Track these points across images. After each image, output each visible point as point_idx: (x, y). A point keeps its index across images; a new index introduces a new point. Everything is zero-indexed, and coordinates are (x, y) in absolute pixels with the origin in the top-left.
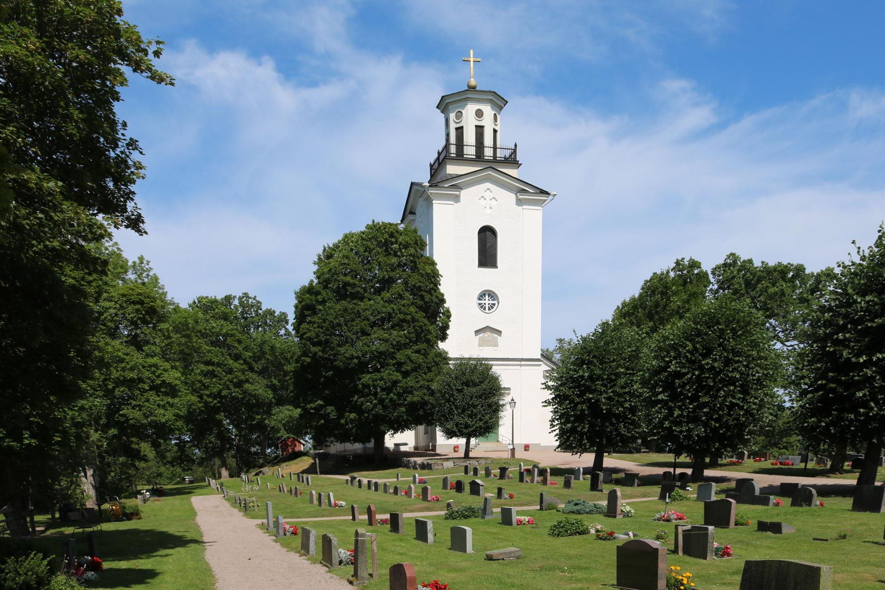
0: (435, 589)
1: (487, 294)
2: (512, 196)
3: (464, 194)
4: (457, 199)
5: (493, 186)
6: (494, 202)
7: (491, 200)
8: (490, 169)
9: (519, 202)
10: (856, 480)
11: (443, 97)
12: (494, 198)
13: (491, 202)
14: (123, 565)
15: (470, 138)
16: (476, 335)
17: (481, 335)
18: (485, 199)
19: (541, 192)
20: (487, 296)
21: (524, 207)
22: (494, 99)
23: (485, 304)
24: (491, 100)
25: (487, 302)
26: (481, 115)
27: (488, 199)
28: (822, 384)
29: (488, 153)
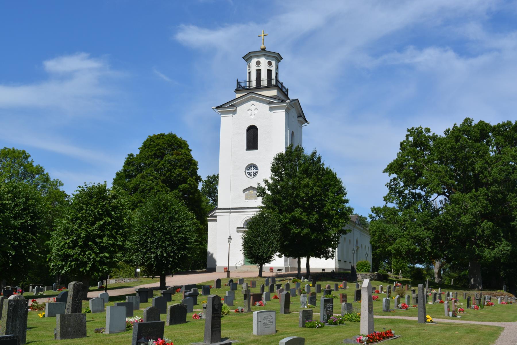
0: (516, 144)
1: (252, 166)
2: (267, 107)
3: (239, 109)
4: (234, 112)
6: (256, 111)
7: (254, 110)
9: (271, 109)
10: (159, 283)
11: (250, 52)
12: (256, 109)
13: (255, 111)
15: (264, 76)
16: (244, 192)
17: (247, 192)
18: (251, 110)
20: (252, 167)
21: (274, 111)
22: (278, 57)
23: (251, 170)
25: (252, 171)
27: (253, 110)
28: (3, 292)
29: (264, 83)
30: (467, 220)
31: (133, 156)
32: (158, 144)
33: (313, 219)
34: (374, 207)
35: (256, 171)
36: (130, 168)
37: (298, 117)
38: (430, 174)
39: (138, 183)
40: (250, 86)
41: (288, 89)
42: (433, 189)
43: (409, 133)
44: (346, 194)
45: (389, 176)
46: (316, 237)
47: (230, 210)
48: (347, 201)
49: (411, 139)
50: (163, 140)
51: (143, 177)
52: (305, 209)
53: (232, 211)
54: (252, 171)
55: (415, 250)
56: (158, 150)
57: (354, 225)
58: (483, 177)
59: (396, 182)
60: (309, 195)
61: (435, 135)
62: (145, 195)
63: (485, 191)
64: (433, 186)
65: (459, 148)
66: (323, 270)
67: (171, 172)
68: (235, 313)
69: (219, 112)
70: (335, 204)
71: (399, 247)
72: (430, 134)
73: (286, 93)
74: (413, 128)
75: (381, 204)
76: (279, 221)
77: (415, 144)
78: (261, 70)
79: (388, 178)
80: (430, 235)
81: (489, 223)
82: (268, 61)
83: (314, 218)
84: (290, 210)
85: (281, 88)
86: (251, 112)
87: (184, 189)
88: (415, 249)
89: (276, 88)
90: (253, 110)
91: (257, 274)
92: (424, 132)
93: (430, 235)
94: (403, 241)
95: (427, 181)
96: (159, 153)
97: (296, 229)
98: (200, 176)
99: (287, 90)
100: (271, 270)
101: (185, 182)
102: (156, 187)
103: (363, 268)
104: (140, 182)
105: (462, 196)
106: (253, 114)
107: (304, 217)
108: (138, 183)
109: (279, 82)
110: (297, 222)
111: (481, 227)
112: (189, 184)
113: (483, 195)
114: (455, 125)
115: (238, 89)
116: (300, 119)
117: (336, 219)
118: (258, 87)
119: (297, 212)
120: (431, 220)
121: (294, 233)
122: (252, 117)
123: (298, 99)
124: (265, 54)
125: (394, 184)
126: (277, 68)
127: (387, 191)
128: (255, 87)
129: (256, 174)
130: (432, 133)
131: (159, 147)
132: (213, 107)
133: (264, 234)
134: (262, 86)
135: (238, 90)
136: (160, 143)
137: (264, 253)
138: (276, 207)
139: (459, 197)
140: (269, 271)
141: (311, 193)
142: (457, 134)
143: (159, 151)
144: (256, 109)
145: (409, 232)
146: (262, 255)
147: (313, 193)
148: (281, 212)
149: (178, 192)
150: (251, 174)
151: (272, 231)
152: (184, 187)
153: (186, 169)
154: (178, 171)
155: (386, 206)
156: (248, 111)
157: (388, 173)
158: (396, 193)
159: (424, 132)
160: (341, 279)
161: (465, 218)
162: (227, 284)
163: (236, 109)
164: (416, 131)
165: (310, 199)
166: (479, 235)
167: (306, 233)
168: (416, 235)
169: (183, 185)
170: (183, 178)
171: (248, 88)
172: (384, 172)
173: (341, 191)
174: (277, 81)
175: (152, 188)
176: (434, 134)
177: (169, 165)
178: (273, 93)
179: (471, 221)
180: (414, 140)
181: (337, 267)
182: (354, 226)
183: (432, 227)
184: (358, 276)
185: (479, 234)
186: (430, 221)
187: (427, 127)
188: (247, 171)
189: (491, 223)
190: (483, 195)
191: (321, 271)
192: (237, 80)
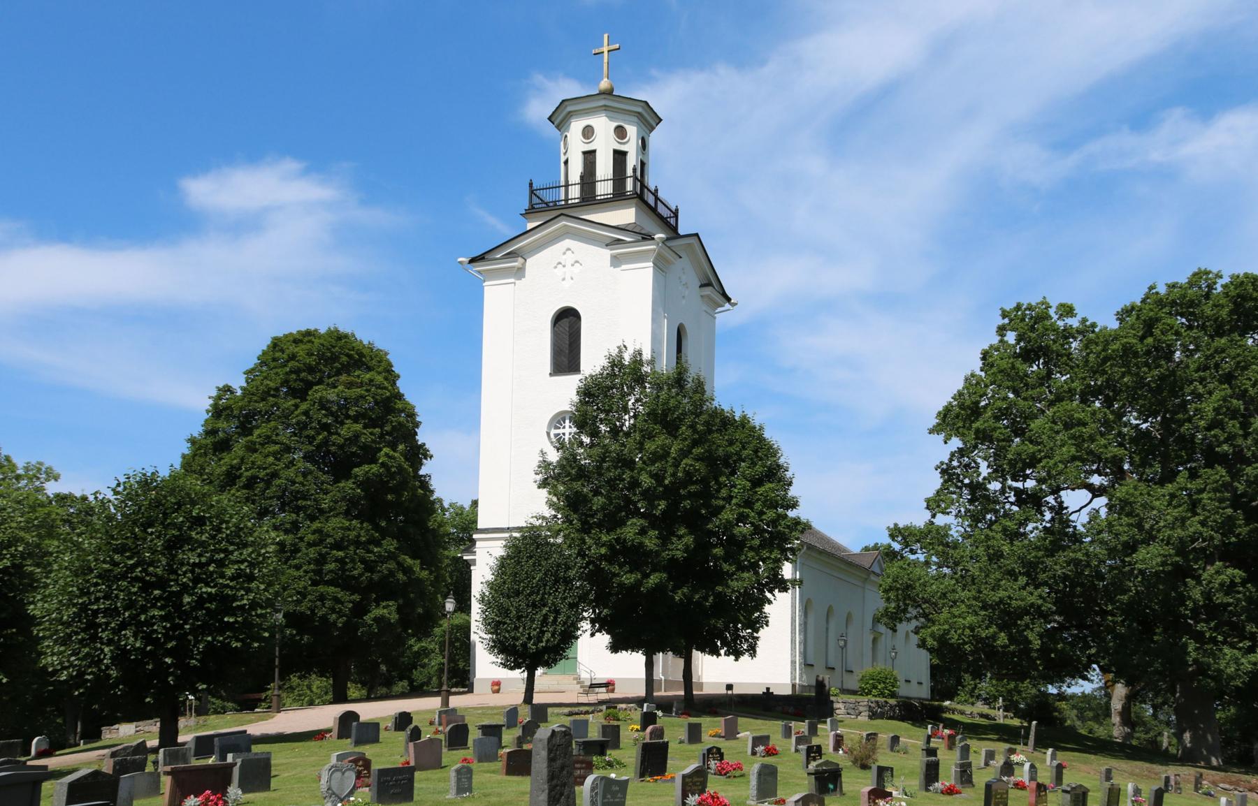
2: (606, 253)
5: (576, 242)
7: (573, 265)
8: (562, 217)
9: (616, 261)
11: (563, 101)
12: (577, 262)
13: (573, 268)
14: (1063, 745)
15: (604, 168)
18: (564, 266)
19: (643, 238)
20: (567, 421)
21: (624, 267)
23: (564, 427)
24: (639, 113)
26: (590, 134)
29: (604, 189)
30: (1151, 559)
31: (232, 393)
32: (293, 357)
33: (679, 547)
34: (896, 525)
36: (222, 425)
37: (702, 286)
38: (1051, 429)
39: (235, 462)
40: (567, 200)
41: (677, 210)
42: (1054, 472)
43: (1006, 321)
44: (791, 482)
45: (946, 443)
46: (689, 599)
47: (507, 532)
48: (794, 505)
49: (1011, 337)
50: (309, 346)
51: (251, 448)
52: (654, 522)
55: (995, 641)
56: (291, 372)
57: (865, 576)
58: (1222, 438)
59: (966, 459)
60: (667, 482)
61: (1088, 323)
62: (255, 495)
63: (1222, 476)
64: (1055, 464)
65: (1148, 353)
66: (729, 687)
67: (330, 434)
69: (479, 272)
70: (752, 509)
71: (945, 630)
72: (1074, 322)
73: (672, 221)
74: (1018, 307)
75: (919, 518)
76: (581, 554)
77: (1028, 355)
78: (594, 151)
79: (943, 449)
80: (1040, 602)
81: (1230, 571)
82: (616, 124)
83: (681, 544)
84: (612, 521)
85: (653, 205)
86: (564, 269)
87: (368, 478)
88: (994, 637)
89: (635, 200)
91: (518, 698)
92: (1055, 317)
93: (1040, 602)
94: (960, 616)
95: (1040, 451)
96: (296, 380)
97: (628, 576)
98: (424, 444)
99: (676, 214)
100: (496, 687)
101: (373, 460)
102: (284, 474)
103: (875, 687)
104: (242, 459)
105: (1145, 492)
106: (568, 278)
107: (651, 541)
108: (235, 462)
109: (649, 190)
110: (634, 556)
111: (1199, 583)
112: (383, 465)
113: (1215, 490)
114: (1151, 288)
115: (533, 208)
116: (708, 291)
117: (751, 548)
119: (630, 531)
120: (1049, 561)
121: (621, 585)
122: (567, 284)
124: (605, 106)
125: (959, 467)
126: (644, 145)
127: (936, 481)
128: (577, 201)
130: (1079, 317)
131: (297, 364)
132: (460, 259)
133: (532, 587)
135: (531, 211)
136: (297, 353)
137: (530, 638)
138: (575, 516)
139: (1132, 495)
140: (488, 689)
141: (674, 475)
142: (1151, 314)
143: (294, 376)
144: (577, 262)
145: (980, 592)
146: (524, 645)
147: (680, 474)
148: (586, 528)
149: (351, 486)
151: (556, 581)
152: (367, 472)
153: (372, 423)
154: (349, 428)
155: (932, 523)
156: (556, 267)
157: (942, 437)
158: (960, 488)
159: (1055, 317)
160: (787, 713)
161: (1148, 553)
162: (390, 725)
163: (524, 264)
164: (1027, 312)
165: (671, 493)
166: (1195, 604)
167: (656, 584)
168: (997, 600)
169: (366, 467)
170: (365, 447)
171: (563, 203)
172: (931, 432)
173: (774, 474)
174: (640, 180)
175: (275, 475)
176: (1084, 320)
177: (324, 412)
178: (626, 215)
179: (1164, 564)
180: (1020, 339)
181: (797, 681)
182: (866, 579)
183: (1050, 578)
184: (836, 705)
185: (1195, 601)
186: (1043, 563)
187: (1063, 301)
188: (553, 432)
189: (1236, 571)
190: (1215, 490)
191: (723, 691)
192: (531, 185)
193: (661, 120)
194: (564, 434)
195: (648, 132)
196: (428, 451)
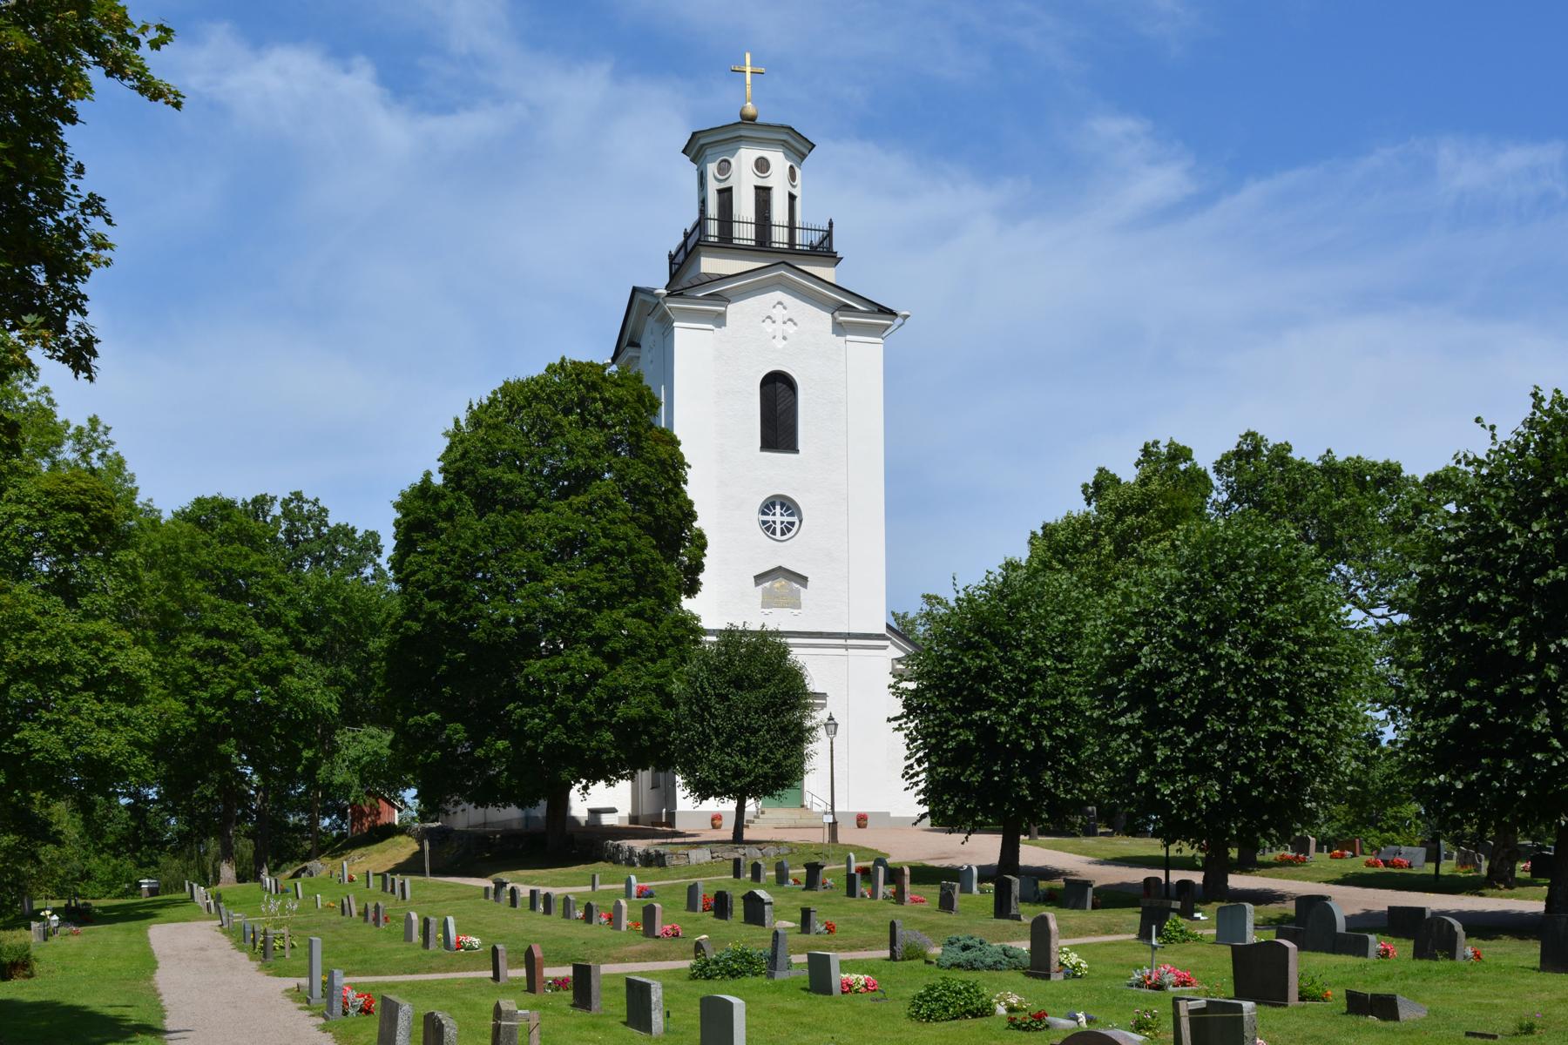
1: (778, 502)
2: (826, 318)
3: (734, 310)
4: (719, 320)
9: (839, 329)
12: (790, 320)
13: (785, 327)
15: (744, 207)
16: (757, 584)
17: (767, 585)
18: (774, 322)
20: (778, 507)
21: (849, 337)
27: (779, 321)
29: (779, 236)
35: (765, 518)
53: (850, 642)
54: (778, 517)
68: (1137, 942)
90: (779, 321)
118: (761, 246)
123: (635, 290)
129: (768, 529)
134: (797, 247)
150: (775, 529)
193: (814, 146)
194: (782, 523)
195: (799, 160)
196: (686, 482)
